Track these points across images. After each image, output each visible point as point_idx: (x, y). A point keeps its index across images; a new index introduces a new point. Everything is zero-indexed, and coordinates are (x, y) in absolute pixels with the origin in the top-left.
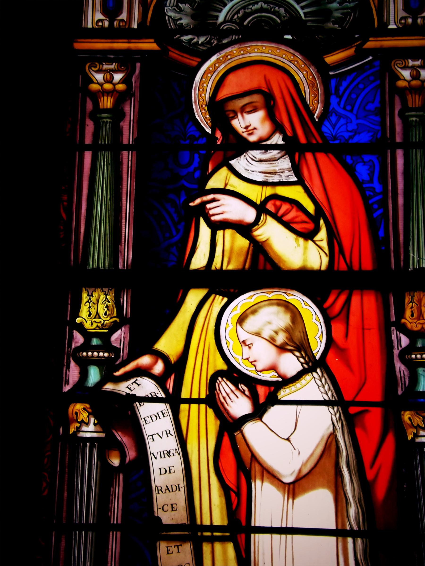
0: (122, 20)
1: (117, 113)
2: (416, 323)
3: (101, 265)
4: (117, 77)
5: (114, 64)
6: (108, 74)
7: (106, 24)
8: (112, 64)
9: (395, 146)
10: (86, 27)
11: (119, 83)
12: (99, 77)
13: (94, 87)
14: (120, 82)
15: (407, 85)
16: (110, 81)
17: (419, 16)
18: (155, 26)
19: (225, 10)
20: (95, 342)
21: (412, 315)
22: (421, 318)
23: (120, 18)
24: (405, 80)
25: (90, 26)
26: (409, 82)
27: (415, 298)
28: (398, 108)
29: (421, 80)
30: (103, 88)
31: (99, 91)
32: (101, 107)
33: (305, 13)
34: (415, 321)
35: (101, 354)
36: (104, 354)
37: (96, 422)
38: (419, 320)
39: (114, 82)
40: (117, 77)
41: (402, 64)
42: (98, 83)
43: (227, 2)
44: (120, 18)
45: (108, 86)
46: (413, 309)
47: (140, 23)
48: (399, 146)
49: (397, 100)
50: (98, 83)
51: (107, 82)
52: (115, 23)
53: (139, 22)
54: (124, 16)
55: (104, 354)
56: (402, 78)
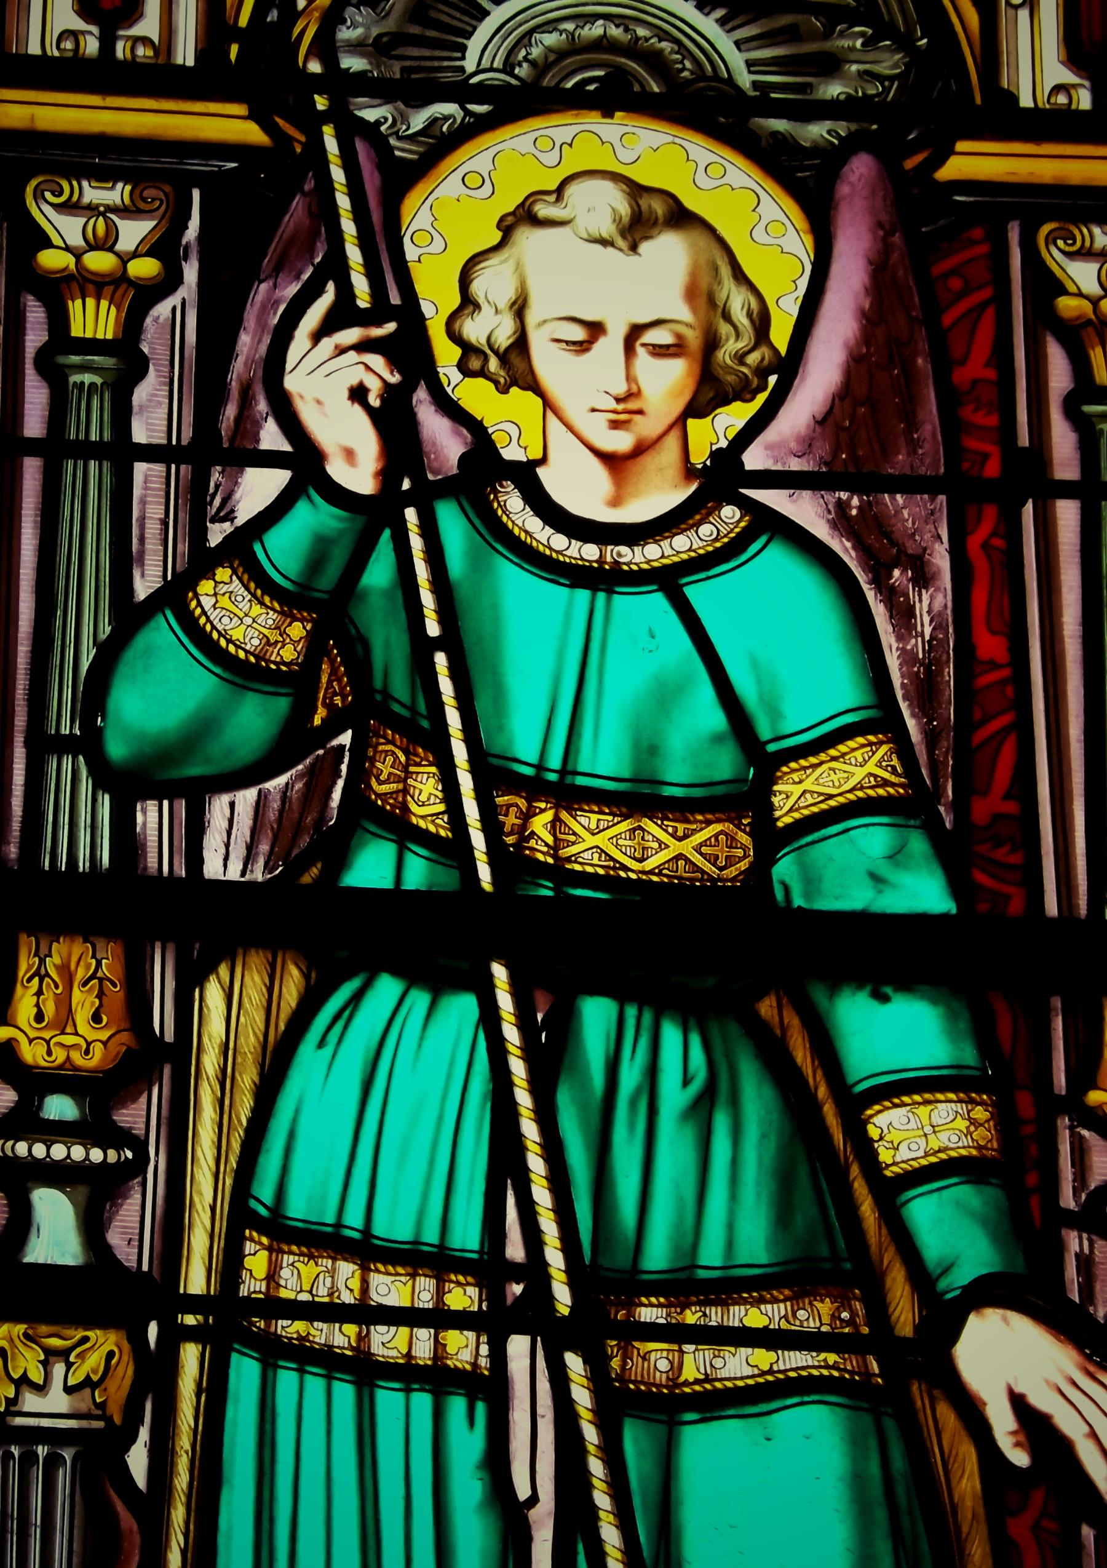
0: (145, 41)
1: (127, 359)
2: (48, 1042)
3: (83, 864)
4: (133, 232)
5: (120, 185)
6: (101, 219)
7: (91, 46)
8: (113, 188)
9: (1050, 490)
10: (22, 51)
11: (135, 255)
12: (70, 229)
13: (51, 260)
14: (144, 249)
15: (72, 266)
16: (106, 243)
17: (121, 33)
18: (246, 61)
19: (485, 29)
20: (59, 1107)
21: (39, 1017)
22: (69, 1030)
23: (137, 30)
24: (1080, 294)
25: (34, 49)
26: (1095, 302)
27: (51, 965)
28: (35, 337)
29: (118, 255)
30: (1101, 312)
31: (1089, 322)
32: (76, 331)
33: (750, 64)
34: (47, 1035)
35: (39, 1150)
36: (48, 1149)
37: (678, 1310)
38: (63, 1033)
39: (119, 247)
40: (133, 232)
41: (61, 194)
42: (67, 249)
43: (487, 5)
44: (137, 30)
45: (99, 262)
46: (42, 997)
47: (201, 50)
48: (1066, 490)
49: (36, 314)
50: (67, 249)
51: (94, 246)
52: (120, 46)
53: (199, 47)
54: (149, 26)
55: (48, 1149)
56: (1072, 288)
